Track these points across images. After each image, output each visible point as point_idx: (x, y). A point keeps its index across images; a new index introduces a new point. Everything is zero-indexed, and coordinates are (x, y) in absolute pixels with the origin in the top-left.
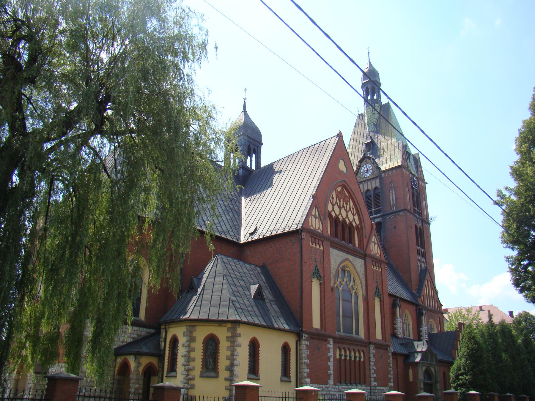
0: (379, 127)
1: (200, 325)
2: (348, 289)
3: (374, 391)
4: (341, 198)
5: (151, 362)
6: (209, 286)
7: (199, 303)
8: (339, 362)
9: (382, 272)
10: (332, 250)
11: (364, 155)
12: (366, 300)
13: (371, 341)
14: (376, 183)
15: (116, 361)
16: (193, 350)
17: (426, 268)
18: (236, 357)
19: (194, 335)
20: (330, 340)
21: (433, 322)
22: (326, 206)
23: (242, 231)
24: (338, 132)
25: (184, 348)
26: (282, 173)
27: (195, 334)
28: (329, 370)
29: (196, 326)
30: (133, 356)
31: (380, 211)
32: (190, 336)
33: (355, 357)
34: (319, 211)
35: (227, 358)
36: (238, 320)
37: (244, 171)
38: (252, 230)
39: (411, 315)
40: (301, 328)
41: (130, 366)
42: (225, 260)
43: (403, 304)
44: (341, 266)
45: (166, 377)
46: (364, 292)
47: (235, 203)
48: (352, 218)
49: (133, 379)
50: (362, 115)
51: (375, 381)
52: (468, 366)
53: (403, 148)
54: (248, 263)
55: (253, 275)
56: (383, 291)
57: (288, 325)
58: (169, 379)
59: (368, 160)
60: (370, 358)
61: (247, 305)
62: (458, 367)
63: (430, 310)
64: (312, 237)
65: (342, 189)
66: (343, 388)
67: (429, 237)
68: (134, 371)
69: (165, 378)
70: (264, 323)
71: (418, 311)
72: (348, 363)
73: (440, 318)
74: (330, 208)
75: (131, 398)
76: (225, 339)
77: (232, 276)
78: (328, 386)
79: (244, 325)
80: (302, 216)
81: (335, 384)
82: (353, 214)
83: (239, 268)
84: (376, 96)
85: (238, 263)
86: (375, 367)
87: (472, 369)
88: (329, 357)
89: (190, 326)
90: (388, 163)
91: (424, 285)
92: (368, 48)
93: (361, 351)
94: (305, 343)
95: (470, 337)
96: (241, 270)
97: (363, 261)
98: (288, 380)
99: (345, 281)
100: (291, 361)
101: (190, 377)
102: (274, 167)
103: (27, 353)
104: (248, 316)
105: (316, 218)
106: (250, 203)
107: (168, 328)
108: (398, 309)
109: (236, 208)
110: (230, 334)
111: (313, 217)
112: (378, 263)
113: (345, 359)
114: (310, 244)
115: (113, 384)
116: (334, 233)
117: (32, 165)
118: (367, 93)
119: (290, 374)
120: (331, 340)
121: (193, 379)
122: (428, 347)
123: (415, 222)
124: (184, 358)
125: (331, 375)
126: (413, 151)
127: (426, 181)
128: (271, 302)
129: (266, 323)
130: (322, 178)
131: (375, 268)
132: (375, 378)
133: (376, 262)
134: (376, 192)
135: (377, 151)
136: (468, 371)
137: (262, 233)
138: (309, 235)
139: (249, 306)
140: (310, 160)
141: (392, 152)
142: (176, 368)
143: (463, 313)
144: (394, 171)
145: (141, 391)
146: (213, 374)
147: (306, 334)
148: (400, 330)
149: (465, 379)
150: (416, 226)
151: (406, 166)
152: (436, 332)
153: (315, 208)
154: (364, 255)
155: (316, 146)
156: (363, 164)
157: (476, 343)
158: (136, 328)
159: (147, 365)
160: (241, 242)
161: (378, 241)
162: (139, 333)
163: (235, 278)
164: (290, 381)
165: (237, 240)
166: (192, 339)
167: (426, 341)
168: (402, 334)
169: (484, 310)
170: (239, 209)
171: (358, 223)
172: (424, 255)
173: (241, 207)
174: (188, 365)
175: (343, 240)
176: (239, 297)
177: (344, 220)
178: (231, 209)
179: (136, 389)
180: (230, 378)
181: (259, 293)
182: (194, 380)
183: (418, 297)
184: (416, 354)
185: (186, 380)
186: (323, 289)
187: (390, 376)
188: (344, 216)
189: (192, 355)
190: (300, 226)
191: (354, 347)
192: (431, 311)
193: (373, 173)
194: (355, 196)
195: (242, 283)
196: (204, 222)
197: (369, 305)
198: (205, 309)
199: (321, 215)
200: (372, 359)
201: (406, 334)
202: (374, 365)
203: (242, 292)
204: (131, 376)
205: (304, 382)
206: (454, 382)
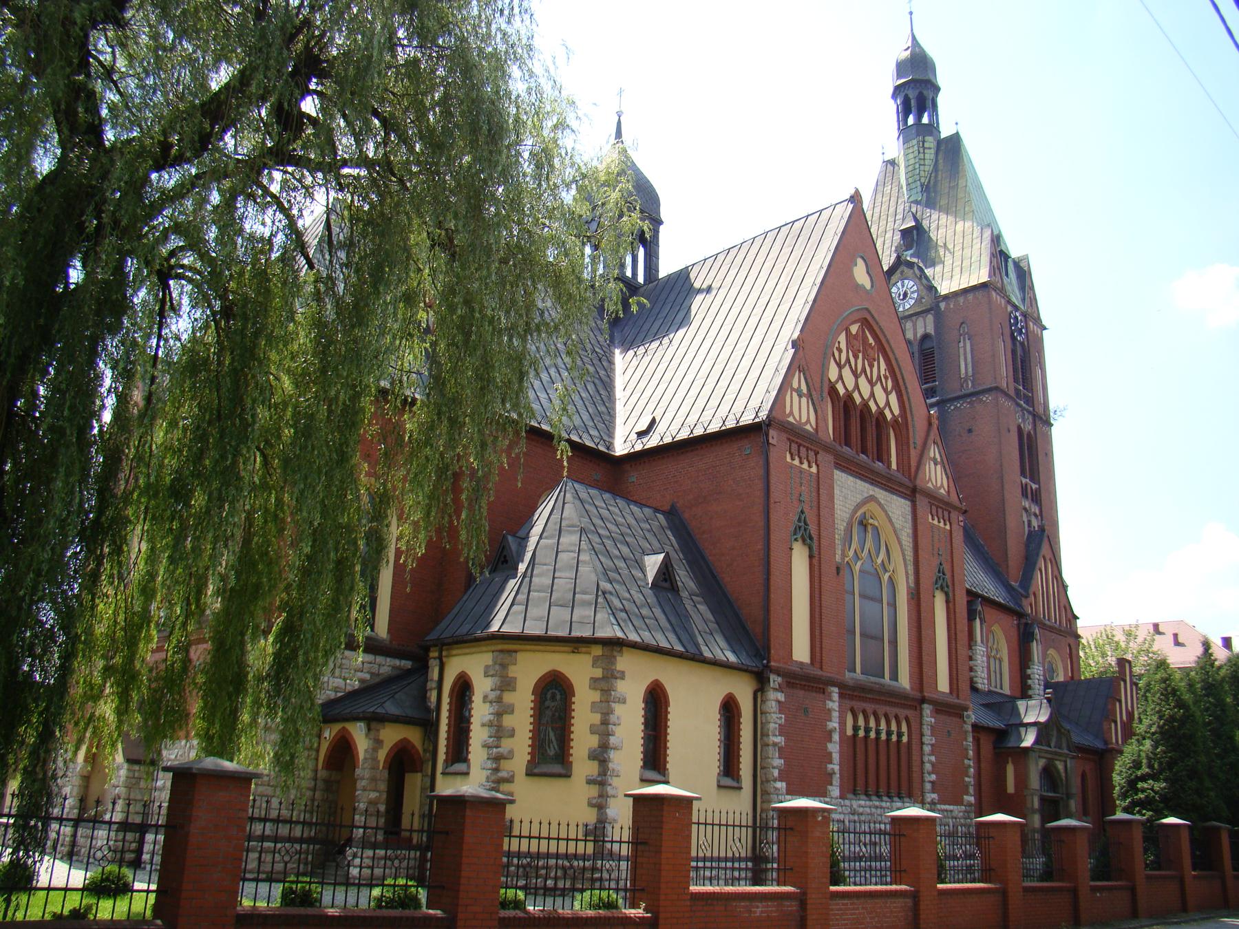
0: (935, 192)
2: (872, 571)
4: (859, 351)
5: (405, 739)
6: (545, 557)
8: (852, 744)
9: (951, 531)
10: (840, 477)
11: (898, 257)
12: (917, 599)
13: (926, 694)
14: (926, 325)
15: (319, 736)
16: (510, 710)
19: (511, 675)
22: (824, 369)
23: (617, 427)
24: (852, 192)
26: (714, 292)
27: (513, 671)
29: (516, 651)
30: (362, 724)
31: (935, 392)
32: (501, 677)
33: (889, 733)
34: (809, 380)
36: (619, 638)
38: (643, 426)
39: (1006, 637)
42: (583, 495)
43: (990, 613)
44: (859, 514)
46: (912, 578)
48: (884, 400)
49: (362, 779)
50: (892, 163)
51: (933, 791)
52: (1159, 759)
53: (992, 240)
54: (636, 503)
56: (953, 576)
57: (734, 652)
58: (450, 779)
59: (906, 270)
60: (922, 735)
61: (638, 604)
62: (1134, 761)
63: (1050, 627)
65: (862, 329)
66: (860, 806)
67: (1049, 455)
68: (365, 759)
69: (439, 776)
70: (679, 648)
71: (1022, 630)
72: (871, 747)
74: (833, 373)
75: (358, 824)
76: (587, 682)
77: (601, 531)
81: (842, 797)
82: (885, 390)
83: (617, 515)
84: (929, 116)
85: (612, 502)
86: (933, 758)
87: (1171, 765)
88: (830, 733)
89: (501, 651)
90: (956, 277)
91: (1037, 567)
93: (902, 717)
94: (774, 697)
95: (1166, 689)
96: (620, 520)
97: (908, 503)
98: (735, 784)
99: (866, 551)
100: (741, 740)
102: (692, 276)
103: (107, 709)
104: (642, 629)
105: (800, 396)
106: (635, 362)
107: (447, 656)
108: (978, 621)
109: (602, 373)
110: (598, 673)
111: (795, 394)
113: (866, 737)
114: (789, 459)
115: (314, 789)
117: (123, 212)
118: (905, 110)
119: (739, 769)
120: (836, 690)
121: (510, 780)
122: (1051, 714)
123: (1020, 420)
124: (486, 728)
125: (834, 773)
126: (1015, 252)
129: (684, 647)
130: (815, 301)
131: (936, 522)
133: (937, 507)
134: (927, 345)
135: (928, 249)
136: (1161, 771)
138: (784, 436)
139: (643, 606)
140: (783, 258)
142: (468, 752)
143: (1116, 639)
144: (970, 296)
145: (382, 808)
146: (557, 769)
147: (779, 675)
148: (983, 672)
149: (1152, 789)
150: (1019, 428)
151: (999, 285)
152: (1061, 678)
153: (800, 371)
154: (912, 491)
155: (798, 225)
156: (894, 278)
157: (1180, 704)
158: (370, 657)
159: (396, 745)
160: (617, 454)
162: (375, 669)
163: (608, 538)
164: (740, 788)
165: (608, 449)
166: (506, 684)
167: (1047, 698)
168: (986, 681)
169: (1163, 634)
170: (609, 376)
171: (897, 412)
172: (1036, 497)
173: (613, 370)
174: (497, 747)
175: (863, 452)
176: (618, 582)
177: (865, 404)
179: (371, 803)
180: (599, 779)
181: (666, 573)
182: (513, 782)
184: (1022, 730)
187: (967, 779)
188: (866, 395)
189: (508, 721)
190: (763, 415)
191: (888, 709)
192: (1051, 629)
193: (919, 301)
195: (625, 550)
197: (922, 609)
200: (927, 739)
201: (993, 684)
203: (625, 572)
204: (358, 772)
205: (772, 790)
206: (1124, 796)
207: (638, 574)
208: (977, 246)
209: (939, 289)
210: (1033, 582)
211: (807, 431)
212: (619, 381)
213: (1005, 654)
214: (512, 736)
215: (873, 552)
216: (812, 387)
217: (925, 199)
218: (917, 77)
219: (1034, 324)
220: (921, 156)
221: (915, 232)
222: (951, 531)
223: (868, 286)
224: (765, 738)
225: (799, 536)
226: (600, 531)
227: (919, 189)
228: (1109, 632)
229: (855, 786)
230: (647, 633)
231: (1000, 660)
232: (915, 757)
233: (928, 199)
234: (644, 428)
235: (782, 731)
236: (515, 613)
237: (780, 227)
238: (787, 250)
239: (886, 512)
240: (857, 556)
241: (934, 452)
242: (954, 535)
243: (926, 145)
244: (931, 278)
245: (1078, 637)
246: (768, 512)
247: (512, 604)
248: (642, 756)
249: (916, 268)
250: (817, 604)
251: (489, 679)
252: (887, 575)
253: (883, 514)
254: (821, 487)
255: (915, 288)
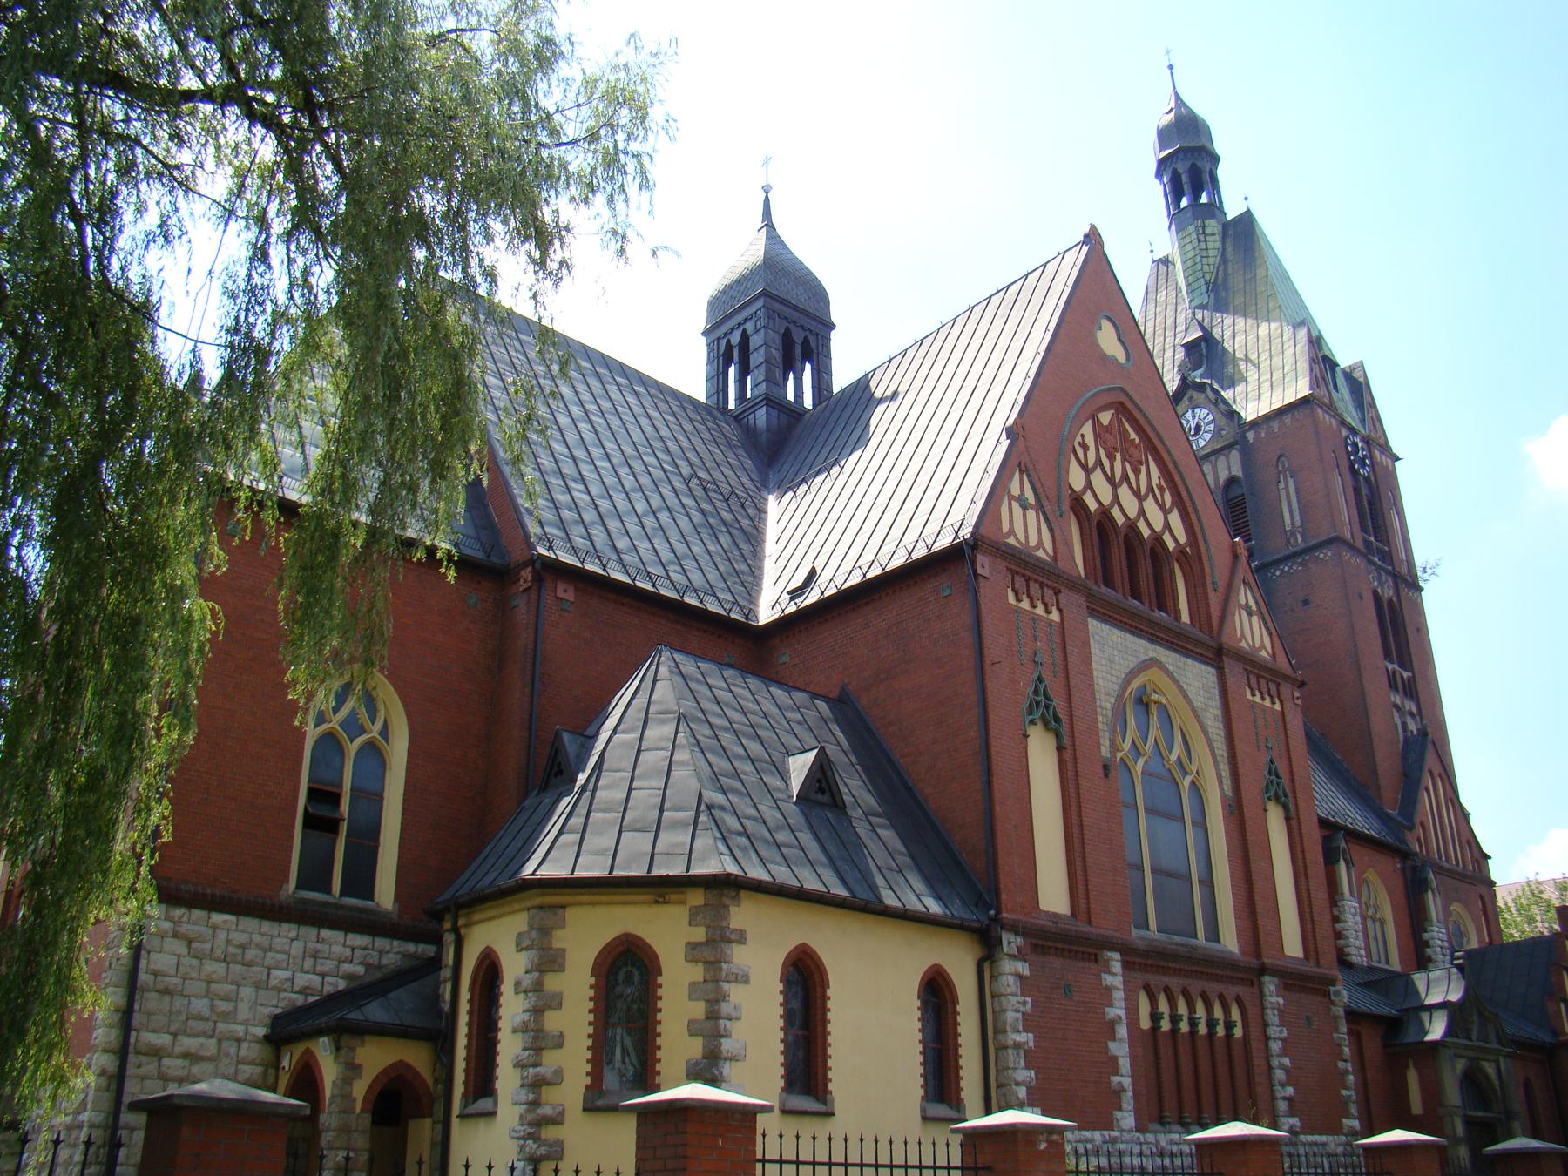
0: (1226, 289)
1: (580, 904)
3: (1292, 1149)
4: (1116, 449)
6: (619, 760)
7: (577, 821)
8: (1150, 1043)
9: (1283, 713)
10: (1094, 625)
11: (1184, 380)
12: (1236, 811)
13: (1265, 960)
14: (1230, 466)
16: (555, 1002)
17: (1423, 733)
18: (728, 1023)
19: (556, 944)
20: (1112, 959)
21: (1464, 914)
24: (1086, 230)
25: (522, 995)
26: (901, 397)
27: (560, 939)
28: (1116, 1072)
29: (564, 906)
33: (1211, 1024)
34: (1038, 485)
35: (693, 1029)
36: (729, 875)
37: (775, 413)
38: (798, 581)
40: (992, 912)
41: (322, 1079)
43: (1360, 853)
44: (1135, 685)
45: (461, 1116)
46: (1227, 783)
47: (743, 506)
49: (328, 1130)
50: (1165, 261)
54: (780, 683)
55: (799, 723)
59: (1195, 394)
60: (1265, 1025)
63: (1448, 870)
64: (1014, 573)
66: (1171, 1142)
67: (1422, 630)
68: (333, 1096)
69: (455, 1121)
70: (839, 891)
72: (1184, 1049)
73: (1484, 895)
74: (1076, 479)
78: (1115, 1133)
79: (754, 894)
80: (973, 501)
81: (1140, 1128)
82: (1161, 506)
83: (746, 699)
84: (1208, 194)
85: (739, 681)
86: (1286, 1061)
88: (1112, 1025)
89: (541, 907)
90: (1266, 395)
91: (1422, 787)
92: (1168, 52)
93: (1230, 997)
94: (1012, 969)
96: (752, 706)
97: (1212, 670)
98: (953, 1114)
99: (1151, 742)
101: (546, 1110)
102: (873, 384)
104: (773, 862)
105: (1025, 507)
107: (468, 925)
108: (1342, 866)
110: (699, 934)
111: (1015, 505)
112: (1268, 681)
113: (1174, 1030)
114: (1011, 599)
116: (1099, 567)
118: (1175, 191)
119: (959, 1089)
120: (1117, 956)
121: (557, 1120)
126: (1344, 360)
127: (1395, 451)
128: (870, 818)
129: (849, 889)
130: (1038, 373)
131: (1258, 699)
132: (1289, 1099)
133: (1258, 677)
134: (1235, 492)
135: (1223, 365)
137: (830, 583)
139: (778, 828)
141: (1274, 359)
143: (1545, 896)
144: (1287, 419)
147: (1017, 933)
150: (1375, 593)
151: (1326, 400)
152: (1474, 944)
153: (1021, 472)
159: (385, 1071)
161: (1262, 604)
162: (374, 958)
163: (725, 729)
166: (549, 961)
167: (1457, 966)
168: (1363, 952)
171: (1182, 539)
172: (1410, 690)
173: (764, 521)
174: (535, 1065)
175: (1134, 597)
177: (1132, 526)
178: (725, 524)
181: (821, 780)
183: (1404, 826)
184: (1425, 1016)
185: (530, 1124)
186: (1070, 766)
187: (1344, 1092)
189: (552, 1021)
190: (966, 532)
193: (1217, 434)
194: (1163, 443)
195: (755, 748)
196: (618, 553)
197: (1248, 829)
198: (601, 840)
199: (1043, 499)
200: (1273, 1031)
201: (1375, 957)
202: (1284, 1053)
203: (751, 778)
207: (774, 781)
208: (1289, 352)
209: (1243, 415)
210: (1419, 807)
211: (1039, 559)
212: (772, 531)
213: (1387, 912)
214: (560, 1045)
215: (1162, 744)
216: (1042, 495)
217: (1212, 301)
218: (1185, 145)
219: (1381, 453)
220: (1203, 245)
221: (1203, 345)
222: (1283, 713)
223: (1122, 358)
224: (1000, 1037)
225: (1037, 716)
226: (713, 720)
227: (1204, 289)
228: (1533, 887)
229: (1161, 1110)
230: (784, 869)
231: (1382, 922)
232: (1258, 1061)
233: (1217, 300)
234: (799, 584)
235: (1028, 1023)
236: (565, 845)
237: (990, 298)
238: (999, 322)
239: (1174, 680)
240: (1137, 751)
241: (1245, 596)
242: (1289, 718)
243: (1208, 231)
244: (1231, 402)
245: (1493, 884)
246: (983, 679)
247: (560, 833)
248: (782, 1071)
249: (1209, 390)
250: (1075, 818)
251: (524, 954)
252: (1187, 780)
253: (1174, 687)
254: (1069, 642)
255: (1210, 417)
